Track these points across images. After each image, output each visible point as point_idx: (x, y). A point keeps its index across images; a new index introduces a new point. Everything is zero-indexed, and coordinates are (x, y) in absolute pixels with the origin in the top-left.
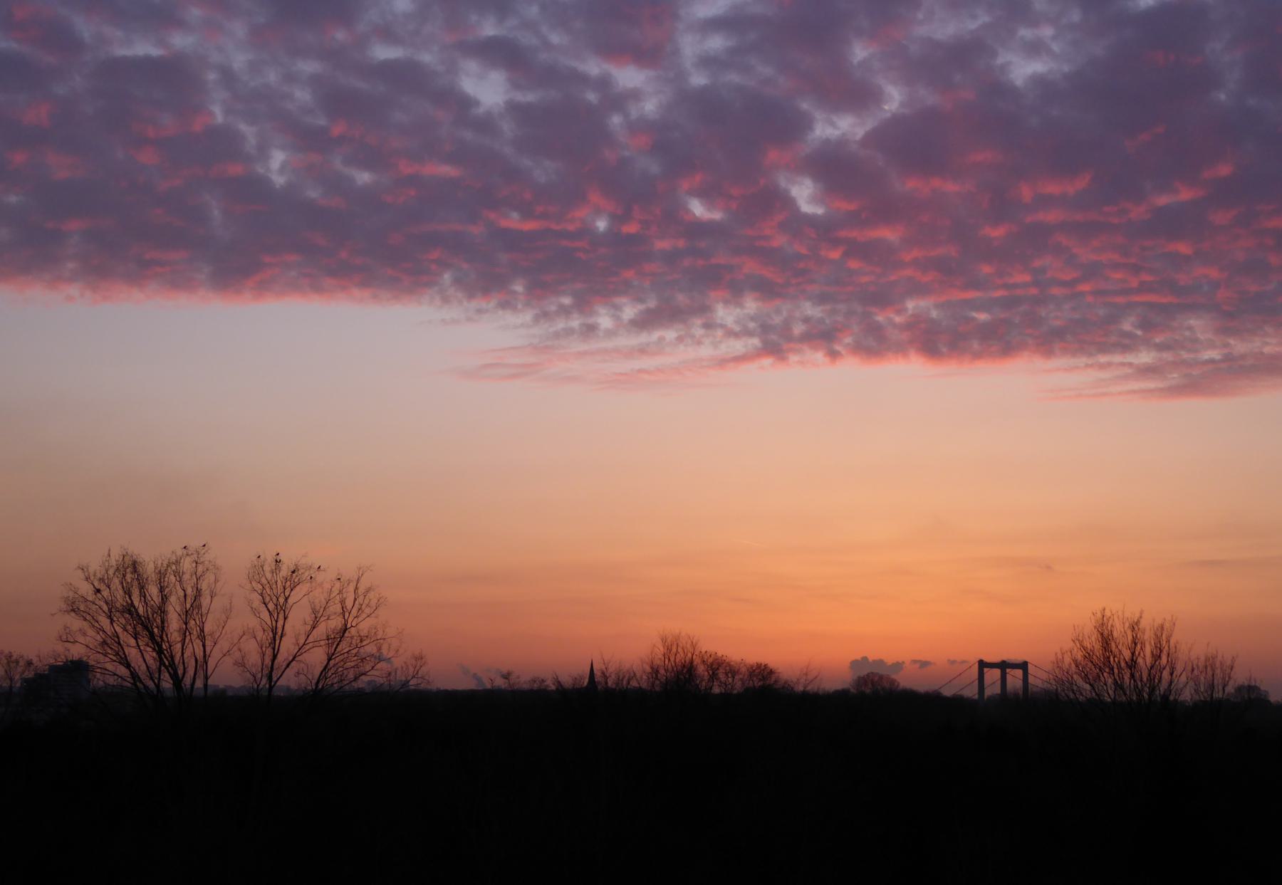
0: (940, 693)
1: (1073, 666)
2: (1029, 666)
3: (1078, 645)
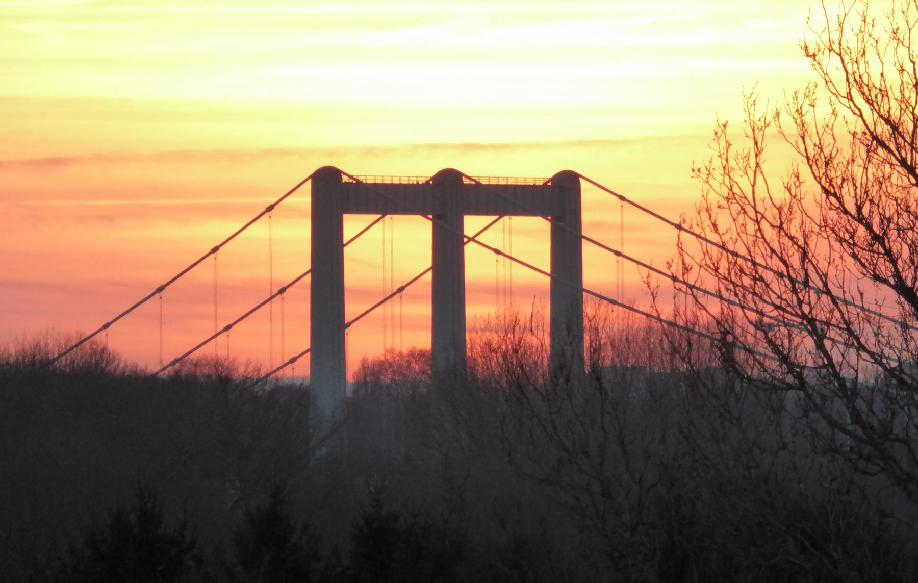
0: (101, 354)
1: (811, 189)
2: (588, 193)
3: (838, 77)
